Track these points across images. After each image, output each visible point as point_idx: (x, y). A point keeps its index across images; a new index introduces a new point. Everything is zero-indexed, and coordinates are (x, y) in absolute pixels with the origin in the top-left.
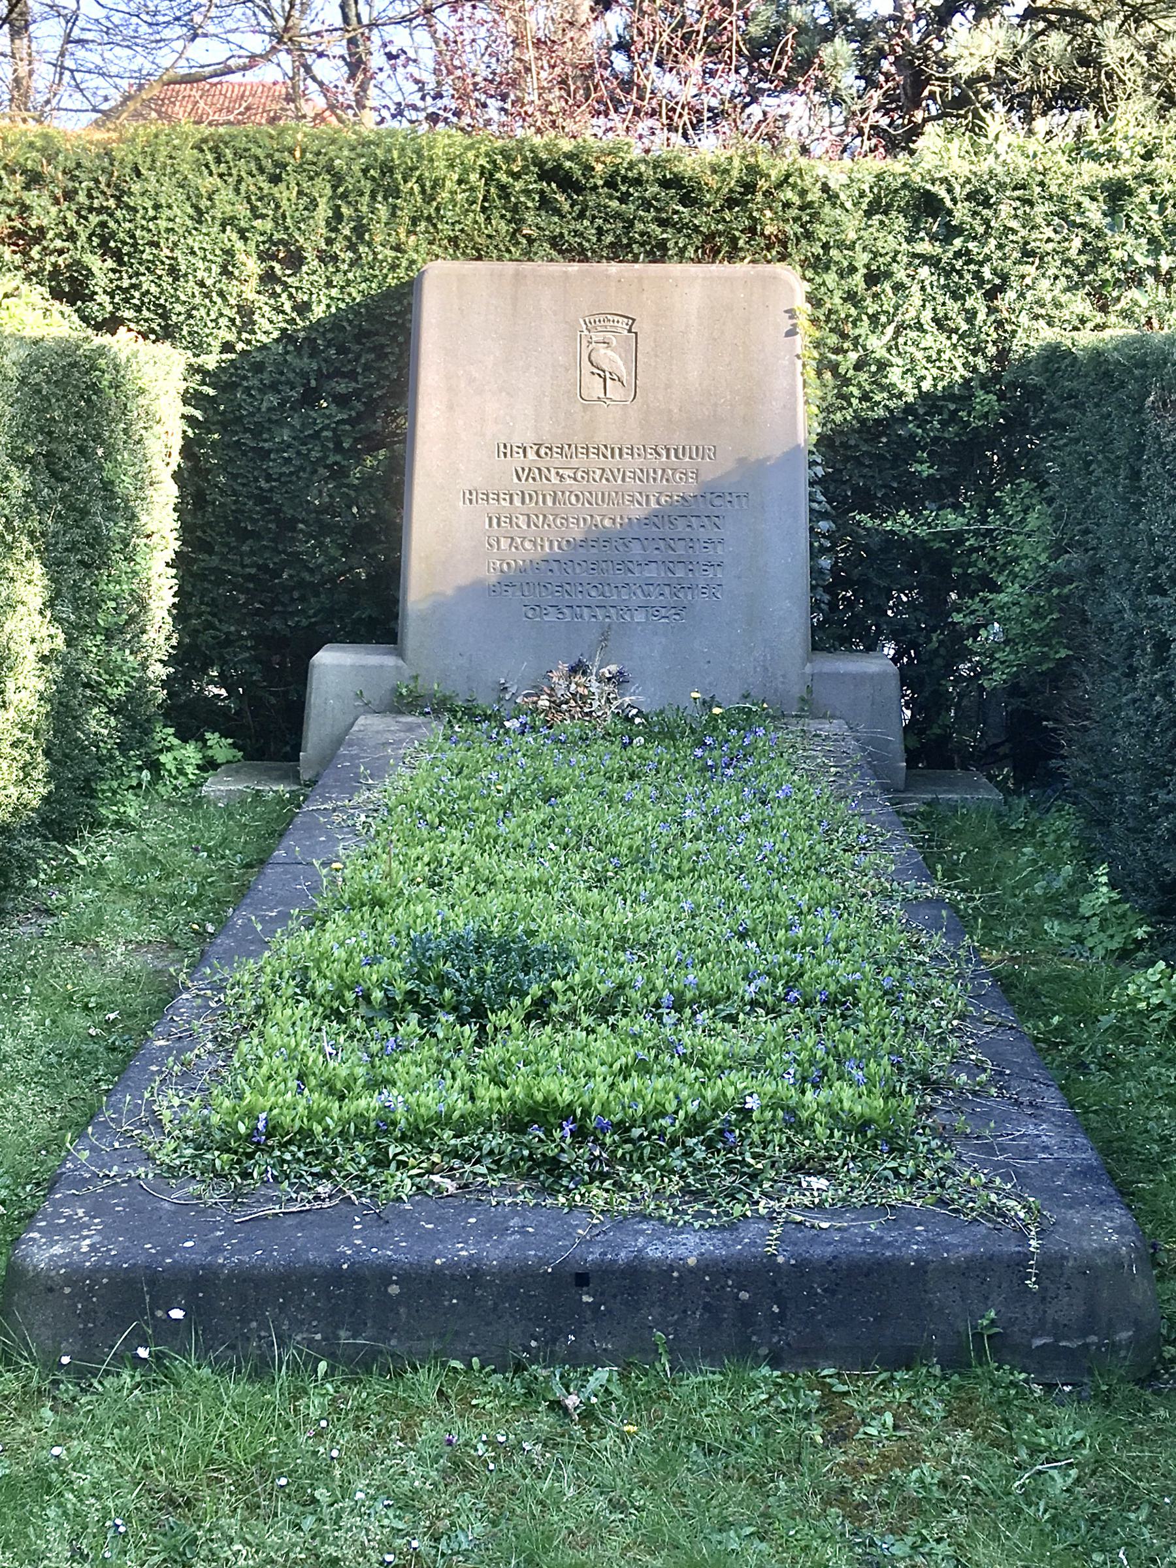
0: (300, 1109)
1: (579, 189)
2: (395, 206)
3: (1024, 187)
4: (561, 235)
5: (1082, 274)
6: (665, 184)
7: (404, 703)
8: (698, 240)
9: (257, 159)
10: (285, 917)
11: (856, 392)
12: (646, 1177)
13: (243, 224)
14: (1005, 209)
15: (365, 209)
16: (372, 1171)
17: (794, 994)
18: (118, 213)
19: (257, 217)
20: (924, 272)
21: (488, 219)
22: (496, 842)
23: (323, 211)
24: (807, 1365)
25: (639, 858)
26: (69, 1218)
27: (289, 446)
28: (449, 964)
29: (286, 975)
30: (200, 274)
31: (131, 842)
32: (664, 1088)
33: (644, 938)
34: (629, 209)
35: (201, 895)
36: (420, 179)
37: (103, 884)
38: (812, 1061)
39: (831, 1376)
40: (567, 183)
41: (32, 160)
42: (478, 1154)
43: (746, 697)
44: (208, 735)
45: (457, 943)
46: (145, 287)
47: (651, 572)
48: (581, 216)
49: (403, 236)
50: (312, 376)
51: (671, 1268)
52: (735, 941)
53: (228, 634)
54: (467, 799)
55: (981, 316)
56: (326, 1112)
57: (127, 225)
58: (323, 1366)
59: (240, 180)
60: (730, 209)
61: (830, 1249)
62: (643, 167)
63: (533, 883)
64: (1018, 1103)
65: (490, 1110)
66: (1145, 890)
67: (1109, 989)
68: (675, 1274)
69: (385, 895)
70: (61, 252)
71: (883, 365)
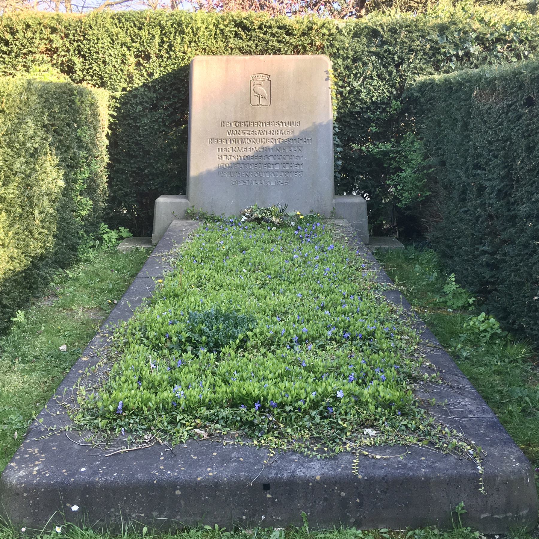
0: (138, 398)
1: (249, 30)
2: (183, 38)
3: (409, 26)
4: (243, 47)
5: (430, 58)
6: (280, 28)
7: (189, 215)
8: (292, 48)
9: (134, 21)
10: (140, 301)
11: (349, 102)
12: (293, 429)
13: (128, 45)
14: (402, 35)
15: (172, 39)
16: (170, 428)
17: (347, 335)
18: (84, 42)
19: (133, 42)
20: (373, 58)
21: (217, 41)
22: (223, 268)
23: (157, 40)
24: (373, 527)
25: (278, 275)
26: (31, 454)
27: (146, 125)
28: (204, 325)
29: (138, 328)
30: (114, 63)
31: (89, 268)
32: (300, 387)
33: (283, 310)
34: (267, 37)
35: (113, 288)
36: (192, 28)
37: (78, 284)
38: (362, 369)
39: (385, 533)
40: (245, 28)
41: (53, 23)
42: (217, 418)
43: (311, 212)
44: (120, 228)
45: (208, 315)
46: (94, 68)
47: (277, 168)
48: (250, 40)
49: (186, 48)
50: (154, 99)
51: (308, 481)
52: (320, 310)
53: (126, 192)
54: (211, 252)
55: (394, 74)
56: (149, 399)
57: (87, 46)
58: (145, 530)
59: (127, 29)
60: (303, 36)
61: (383, 471)
62: (272, 22)
63: (238, 286)
64: (452, 387)
65: (222, 397)
66: (471, 284)
67: (462, 323)
68: (310, 484)
69: (179, 293)
70: (64, 56)
71: (359, 92)
